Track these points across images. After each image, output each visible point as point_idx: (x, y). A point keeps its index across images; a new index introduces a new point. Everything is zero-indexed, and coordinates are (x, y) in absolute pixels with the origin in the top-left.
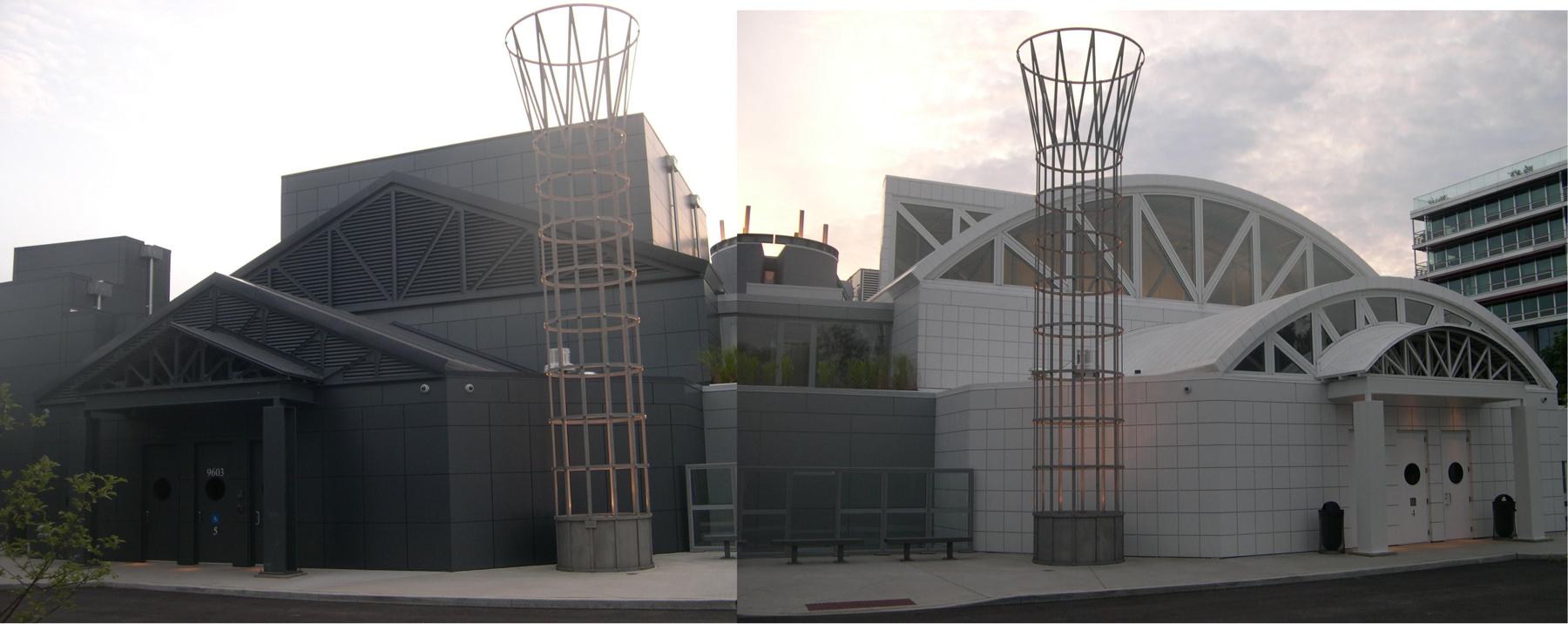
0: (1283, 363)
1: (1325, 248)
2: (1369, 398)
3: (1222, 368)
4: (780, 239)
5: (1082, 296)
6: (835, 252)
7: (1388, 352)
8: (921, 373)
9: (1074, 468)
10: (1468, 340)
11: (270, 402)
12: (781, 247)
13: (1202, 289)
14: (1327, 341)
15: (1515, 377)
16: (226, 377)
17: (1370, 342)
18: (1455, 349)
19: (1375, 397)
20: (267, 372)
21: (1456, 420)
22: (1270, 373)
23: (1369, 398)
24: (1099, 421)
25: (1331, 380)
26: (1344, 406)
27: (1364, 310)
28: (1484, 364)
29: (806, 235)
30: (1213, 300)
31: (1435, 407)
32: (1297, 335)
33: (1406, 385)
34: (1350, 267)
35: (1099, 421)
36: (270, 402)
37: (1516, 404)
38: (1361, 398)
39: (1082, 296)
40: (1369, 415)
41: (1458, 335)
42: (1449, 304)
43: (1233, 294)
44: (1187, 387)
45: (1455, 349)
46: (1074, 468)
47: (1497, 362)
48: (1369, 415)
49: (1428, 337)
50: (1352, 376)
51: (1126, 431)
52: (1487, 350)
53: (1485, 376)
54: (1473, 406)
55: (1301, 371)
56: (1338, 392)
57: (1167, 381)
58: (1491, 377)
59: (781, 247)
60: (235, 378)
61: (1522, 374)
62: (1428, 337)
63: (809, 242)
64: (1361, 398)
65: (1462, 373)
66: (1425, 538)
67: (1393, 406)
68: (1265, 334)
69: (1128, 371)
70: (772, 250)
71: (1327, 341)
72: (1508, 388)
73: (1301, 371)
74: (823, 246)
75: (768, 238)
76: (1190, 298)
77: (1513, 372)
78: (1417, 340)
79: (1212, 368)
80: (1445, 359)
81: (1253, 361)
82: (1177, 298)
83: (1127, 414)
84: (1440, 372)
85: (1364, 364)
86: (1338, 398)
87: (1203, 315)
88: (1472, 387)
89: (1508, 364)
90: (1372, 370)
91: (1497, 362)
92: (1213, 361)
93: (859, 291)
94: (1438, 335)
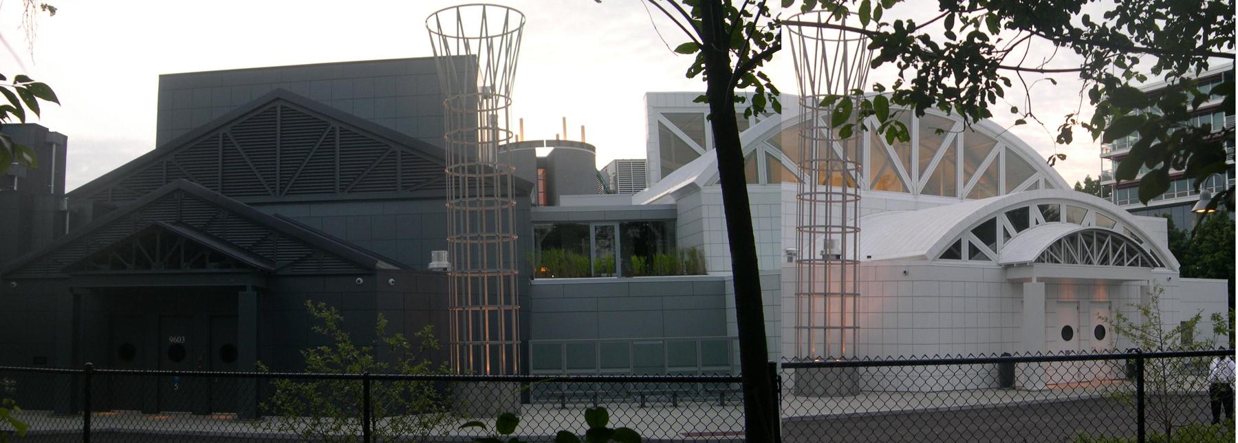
0: (974, 252)
1: (1014, 149)
2: (1034, 281)
3: (930, 257)
4: (549, 143)
5: (804, 97)
6: (593, 148)
7: (1051, 248)
8: (708, 259)
9: (825, 295)
10: (1109, 238)
11: (244, 288)
12: (551, 149)
13: (917, 183)
14: (1007, 236)
15: (1144, 264)
16: (203, 266)
17: (1041, 236)
18: (1101, 242)
19: (1040, 280)
20: (240, 264)
21: (1101, 294)
22: (965, 261)
23: (1034, 281)
24: (843, 295)
25: (1008, 266)
26: (1017, 284)
27: (1035, 214)
28: (1121, 254)
29: (569, 138)
30: (924, 192)
31: (1087, 286)
32: (986, 231)
33: (1063, 270)
34: (1035, 166)
35: (843, 295)
36: (244, 288)
37: (1145, 283)
38: (1029, 280)
39: (804, 97)
40: (1034, 293)
41: (1102, 235)
42: (1101, 209)
43: (940, 186)
44: (904, 270)
45: (1101, 242)
46: (825, 295)
47: (1131, 252)
48: (1034, 293)
49: (1080, 236)
50: (1022, 265)
51: (861, 301)
52: (1124, 245)
53: (1121, 264)
54: (1114, 285)
55: (987, 258)
56: (1015, 274)
57: (892, 264)
58: (1126, 264)
59: (551, 149)
60: (212, 268)
61: (1149, 261)
62: (1080, 236)
63: (572, 143)
64: (1029, 280)
65: (1104, 261)
66: (783, 345)
67: (1052, 285)
68: (963, 233)
69: (862, 258)
70: (543, 152)
71: (1007, 236)
72: (1138, 273)
73: (987, 258)
74: (583, 145)
75: (540, 143)
76: (906, 190)
77: (1143, 260)
78: (1072, 238)
79: (923, 258)
80: (1092, 252)
81: (952, 252)
82: (898, 190)
83: (861, 290)
84: (1089, 261)
85: (1031, 255)
86: (1013, 278)
87: (916, 207)
88: (1112, 272)
89: (1139, 255)
90: (1040, 260)
91: (1131, 252)
92: (924, 252)
93: (615, 178)
94: (1088, 234)
